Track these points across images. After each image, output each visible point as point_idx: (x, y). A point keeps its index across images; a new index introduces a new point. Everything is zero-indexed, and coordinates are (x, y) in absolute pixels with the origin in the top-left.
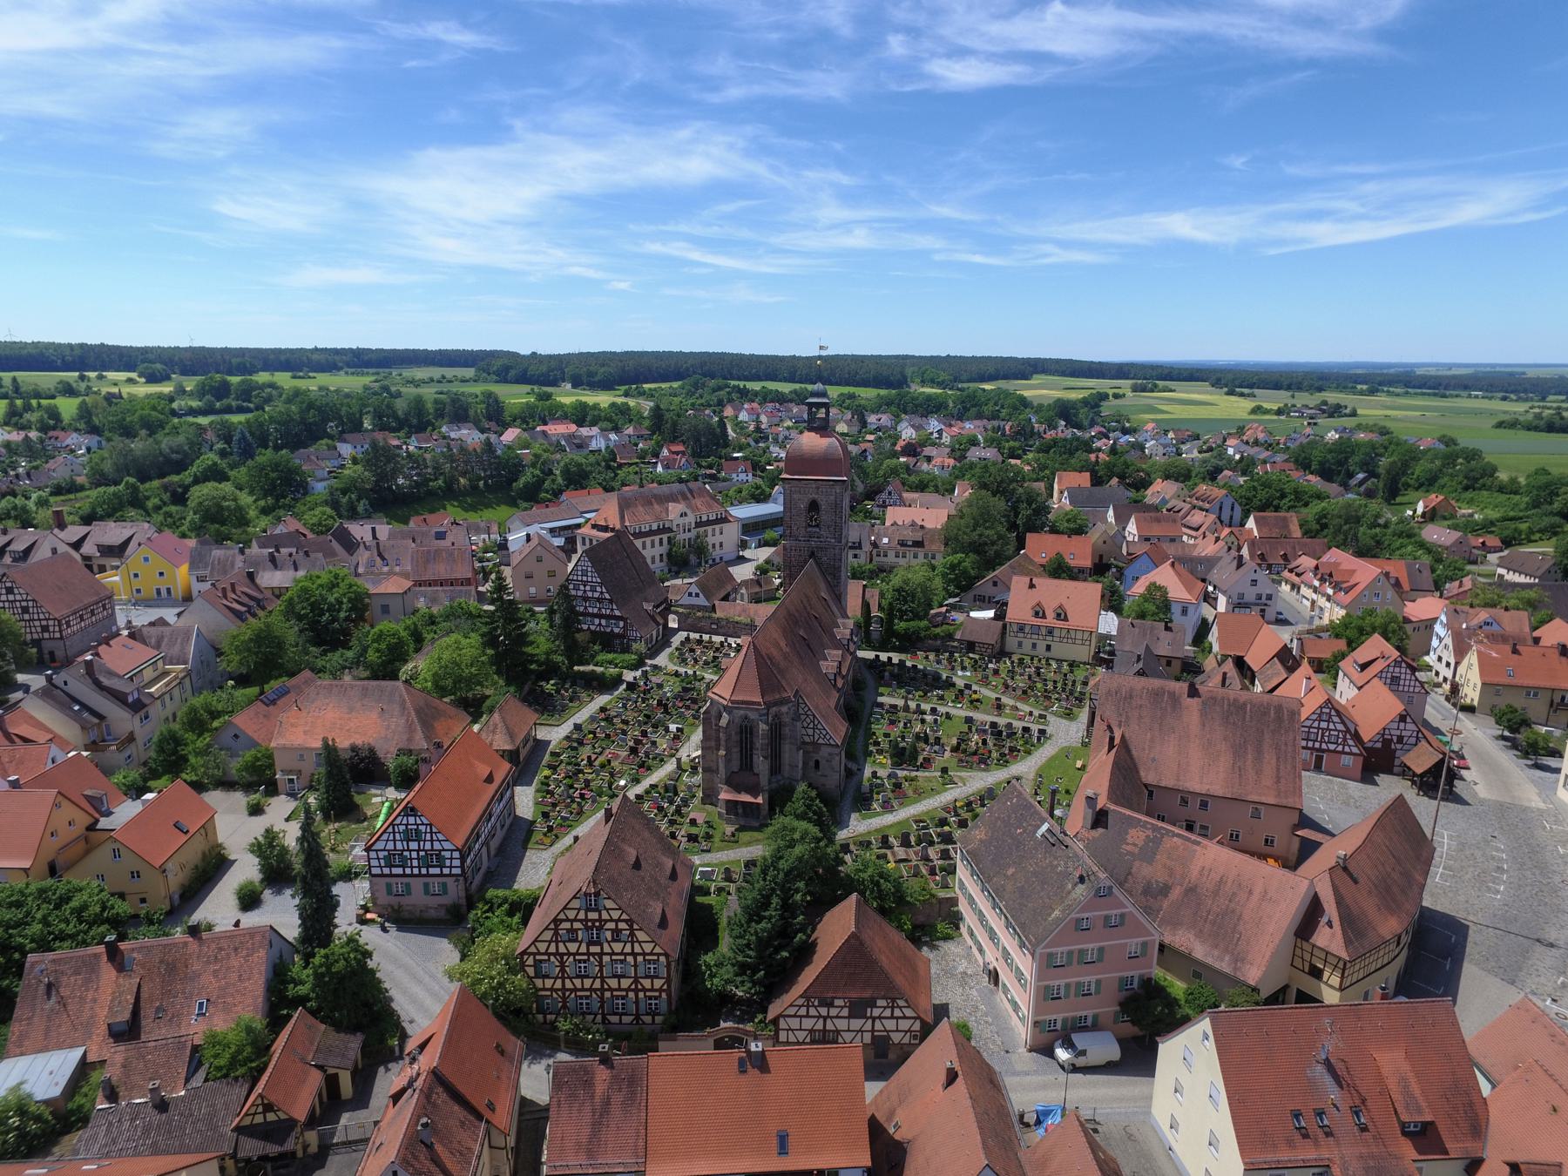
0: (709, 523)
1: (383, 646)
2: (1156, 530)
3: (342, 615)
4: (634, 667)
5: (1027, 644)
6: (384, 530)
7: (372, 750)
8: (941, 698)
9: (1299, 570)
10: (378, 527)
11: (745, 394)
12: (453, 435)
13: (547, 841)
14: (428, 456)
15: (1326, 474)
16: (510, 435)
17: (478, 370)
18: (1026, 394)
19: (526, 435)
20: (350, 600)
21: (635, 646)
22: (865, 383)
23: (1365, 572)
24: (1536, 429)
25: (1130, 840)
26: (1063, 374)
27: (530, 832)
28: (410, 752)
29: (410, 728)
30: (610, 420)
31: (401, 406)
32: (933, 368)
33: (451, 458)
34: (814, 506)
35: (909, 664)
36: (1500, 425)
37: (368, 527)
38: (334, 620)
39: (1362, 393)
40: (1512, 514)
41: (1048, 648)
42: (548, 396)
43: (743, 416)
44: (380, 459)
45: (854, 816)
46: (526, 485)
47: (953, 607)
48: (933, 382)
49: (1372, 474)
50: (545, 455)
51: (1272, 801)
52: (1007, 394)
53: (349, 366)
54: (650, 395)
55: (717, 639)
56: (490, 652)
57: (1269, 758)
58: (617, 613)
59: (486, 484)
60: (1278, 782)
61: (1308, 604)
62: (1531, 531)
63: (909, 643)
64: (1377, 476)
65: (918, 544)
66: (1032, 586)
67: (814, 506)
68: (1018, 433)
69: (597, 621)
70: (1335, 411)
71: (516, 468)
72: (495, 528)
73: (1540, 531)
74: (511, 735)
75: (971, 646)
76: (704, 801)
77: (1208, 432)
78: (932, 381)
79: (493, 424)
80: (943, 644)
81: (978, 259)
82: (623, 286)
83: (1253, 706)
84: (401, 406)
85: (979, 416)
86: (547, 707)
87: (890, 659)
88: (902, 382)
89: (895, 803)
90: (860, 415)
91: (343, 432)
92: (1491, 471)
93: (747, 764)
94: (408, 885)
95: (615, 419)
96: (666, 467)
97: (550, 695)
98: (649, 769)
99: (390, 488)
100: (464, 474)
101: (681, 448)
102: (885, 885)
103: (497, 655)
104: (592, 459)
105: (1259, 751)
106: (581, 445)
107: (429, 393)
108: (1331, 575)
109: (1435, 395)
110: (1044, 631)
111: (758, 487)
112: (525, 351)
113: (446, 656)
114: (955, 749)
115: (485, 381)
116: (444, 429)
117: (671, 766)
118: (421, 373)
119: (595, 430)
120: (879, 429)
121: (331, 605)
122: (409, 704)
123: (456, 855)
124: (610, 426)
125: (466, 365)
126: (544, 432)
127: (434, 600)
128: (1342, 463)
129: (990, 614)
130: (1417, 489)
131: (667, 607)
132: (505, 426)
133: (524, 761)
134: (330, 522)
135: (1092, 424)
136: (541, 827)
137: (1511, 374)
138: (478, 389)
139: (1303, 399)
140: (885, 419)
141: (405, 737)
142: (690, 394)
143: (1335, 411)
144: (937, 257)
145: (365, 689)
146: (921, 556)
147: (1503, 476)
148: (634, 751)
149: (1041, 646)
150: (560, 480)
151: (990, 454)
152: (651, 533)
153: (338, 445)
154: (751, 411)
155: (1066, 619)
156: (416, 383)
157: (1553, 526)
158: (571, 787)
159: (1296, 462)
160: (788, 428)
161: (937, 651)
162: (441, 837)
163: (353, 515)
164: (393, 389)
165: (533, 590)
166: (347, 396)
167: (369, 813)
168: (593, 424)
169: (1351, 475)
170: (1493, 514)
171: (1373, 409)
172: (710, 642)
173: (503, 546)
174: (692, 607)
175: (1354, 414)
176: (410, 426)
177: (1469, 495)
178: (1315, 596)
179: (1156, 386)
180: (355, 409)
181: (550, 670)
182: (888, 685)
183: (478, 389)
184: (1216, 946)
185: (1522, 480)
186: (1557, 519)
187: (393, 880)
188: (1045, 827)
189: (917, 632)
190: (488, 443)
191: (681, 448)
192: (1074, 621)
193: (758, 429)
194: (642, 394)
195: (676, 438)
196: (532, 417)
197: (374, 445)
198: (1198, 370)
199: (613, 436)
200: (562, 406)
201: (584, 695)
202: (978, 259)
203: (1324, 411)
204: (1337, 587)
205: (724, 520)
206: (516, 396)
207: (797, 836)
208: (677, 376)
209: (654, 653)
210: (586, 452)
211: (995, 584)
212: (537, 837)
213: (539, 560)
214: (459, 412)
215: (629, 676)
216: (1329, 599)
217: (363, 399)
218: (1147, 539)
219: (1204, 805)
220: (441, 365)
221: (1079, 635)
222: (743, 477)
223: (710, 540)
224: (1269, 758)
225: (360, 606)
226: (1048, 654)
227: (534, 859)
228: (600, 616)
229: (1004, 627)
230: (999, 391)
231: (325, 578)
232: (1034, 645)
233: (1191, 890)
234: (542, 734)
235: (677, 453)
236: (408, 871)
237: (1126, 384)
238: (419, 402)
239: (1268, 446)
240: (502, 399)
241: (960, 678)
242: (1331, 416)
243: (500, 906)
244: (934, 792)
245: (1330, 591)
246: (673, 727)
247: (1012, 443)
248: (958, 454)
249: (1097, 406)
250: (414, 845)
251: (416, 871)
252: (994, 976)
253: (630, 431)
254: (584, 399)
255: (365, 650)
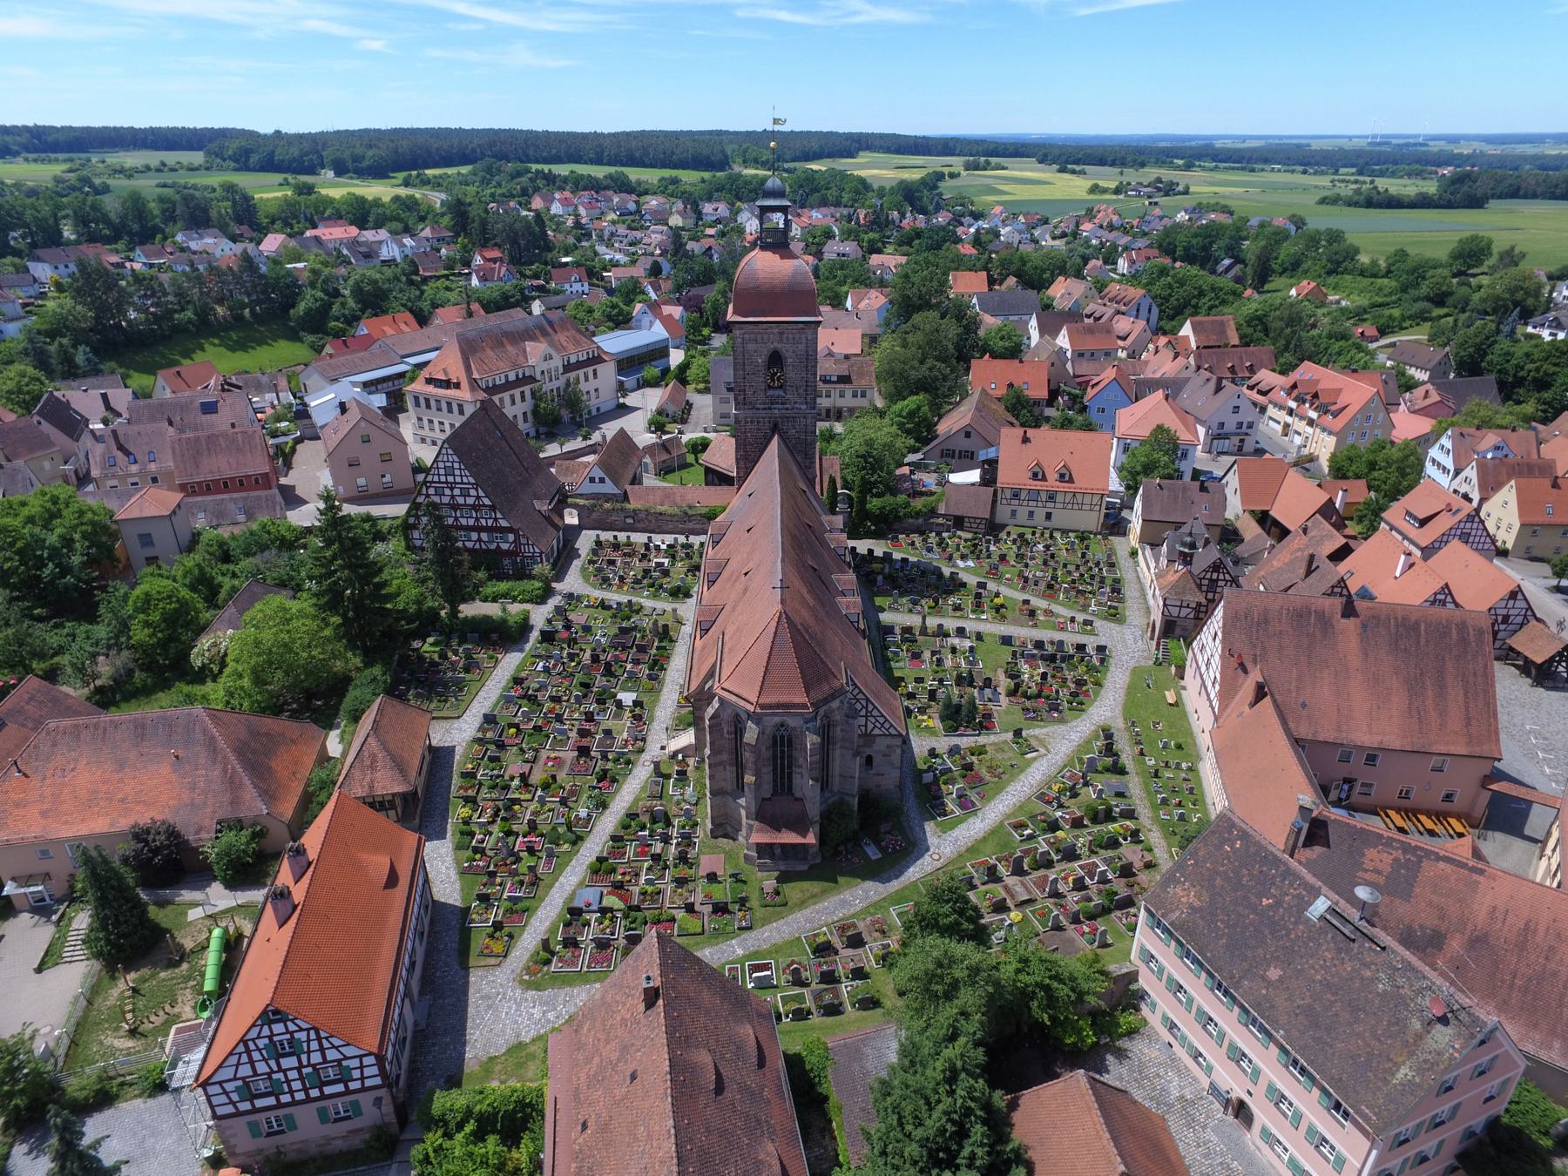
0: (580, 365)
1: (155, 617)
2: (1090, 344)
3: (76, 560)
4: (541, 600)
5: (1022, 514)
6: (121, 398)
7: (173, 834)
8: (957, 608)
9: (1263, 386)
10: (110, 392)
11: (550, 179)
12: (194, 245)
13: (498, 947)
14: (165, 278)
15: (1189, 258)
16: (272, 243)
17: (208, 153)
18: (862, 173)
19: (293, 243)
20: (85, 536)
21: (537, 569)
22: (682, 165)
23: (1356, 392)
24: (1356, 204)
25: (1368, 865)
26: (888, 151)
27: (465, 934)
28: (239, 825)
29: (233, 785)
30: (397, 218)
31: (112, 205)
32: (752, 144)
33: (199, 280)
34: (775, 359)
35: (879, 553)
36: (1323, 201)
37: (96, 394)
38: (65, 570)
39: (1178, 168)
40: (1380, 300)
41: (1049, 516)
42: (309, 190)
43: (556, 209)
44: (92, 284)
45: (929, 827)
46: (308, 312)
47: (916, 466)
48: (757, 163)
49: (1238, 260)
50: (327, 271)
51: (1462, 750)
52: (843, 175)
53: (28, 151)
54: (436, 184)
55: (639, 538)
56: (336, 620)
57: (1455, 694)
58: (504, 523)
59: (253, 312)
60: (1468, 724)
61: (1279, 428)
62: (1404, 318)
63: (886, 525)
64: (1243, 262)
65: (845, 379)
66: (1026, 440)
67: (775, 359)
68: (873, 222)
69: (474, 536)
70: (1169, 189)
71: (289, 290)
72: (283, 383)
73: (1410, 317)
74: (400, 767)
75: (959, 522)
76: (715, 835)
77: (1057, 215)
78: (756, 161)
79: (245, 228)
80: (924, 523)
81: (784, 16)
82: (377, 45)
83: (1428, 625)
84: (112, 205)
85: (824, 203)
86: (428, 684)
87: (871, 551)
88: (723, 164)
89: (972, 796)
90: (693, 204)
91: (34, 245)
92: (1352, 253)
93: (782, 783)
94: (289, 1118)
95: (404, 217)
96: (483, 279)
97: (433, 664)
98: (614, 780)
99: (118, 326)
100: (220, 301)
101: (496, 254)
102: (1063, 991)
103: (347, 621)
104: (388, 272)
105: (1441, 687)
106: (369, 254)
107: (147, 186)
108: (1315, 396)
109: (1243, 169)
110: (1044, 496)
111: (614, 306)
112: (265, 128)
113: (267, 636)
114: (1012, 693)
115: (221, 169)
116: (179, 238)
117: (641, 774)
118: (132, 159)
119: (383, 234)
120: (718, 221)
121: (53, 549)
122: (222, 744)
123: (370, 1060)
124: (400, 226)
125: (190, 146)
126: (317, 238)
127: (219, 517)
128: (1206, 248)
129: (974, 476)
130: (1281, 274)
131: (562, 499)
132: (261, 231)
133: (420, 809)
134: (36, 387)
135: (938, 209)
136: (482, 922)
137: (1298, 146)
138: (215, 179)
139: (1132, 176)
140: (723, 209)
141: (227, 798)
142: (485, 182)
143: (1169, 189)
144: (740, 14)
145: (140, 729)
146: (849, 394)
147: (1364, 259)
148: (584, 751)
149: (1040, 515)
150: (351, 303)
151: (849, 248)
152: (508, 386)
153: (31, 265)
154: (565, 202)
155: (1071, 481)
156: (129, 173)
157: (1423, 311)
158: (509, 833)
159: (1160, 247)
160: (613, 222)
161: (921, 532)
162: (336, 1042)
163: (71, 372)
164: (97, 181)
165: (361, 481)
166: (32, 193)
167: (188, 944)
168: (378, 225)
169: (1217, 261)
170: (1363, 301)
171: (1204, 185)
172: (629, 544)
173: (302, 414)
174: (596, 496)
175: (1186, 192)
176: (130, 234)
177: (1332, 280)
178: (1289, 419)
179: (988, 163)
180: (46, 210)
181: (427, 622)
182: (885, 593)
183: (215, 179)
184: (1535, 1026)
185: (1382, 263)
186: (1426, 305)
187: (263, 1116)
188: (1320, 906)
189: (894, 511)
190: (247, 259)
191: (496, 254)
192: (1081, 483)
193: (578, 225)
194: (426, 182)
195: (487, 241)
196: (295, 217)
197: (82, 266)
198: (1024, 145)
199: (408, 241)
200: (331, 201)
201: (482, 656)
202: (784, 16)
203: (1159, 189)
204: (1323, 410)
205: (596, 359)
206: (269, 191)
207: (959, 973)
208: (464, 159)
209: (560, 571)
210: (377, 262)
211: (968, 435)
212: (479, 941)
213: (366, 440)
214: (199, 219)
215: (540, 616)
216: (1311, 423)
217: (61, 189)
218: (1081, 355)
219: (1371, 759)
220: (157, 148)
221: (1087, 499)
222: (577, 287)
223: (583, 386)
224: (1455, 694)
225: (106, 551)
226: (1048, 524)
227: (486, 990)
228: (479, 529)
229: (995, 492)
230: (833, 173)
231: (35, 506)
232: (1031, 514)
233: (1478, 941)
234: (440, 735)
235: (494, 260)
236: (285, 1098)
237: (957, 163)
238: (136, 204)
239: (1125, 230)
240: (250, 192)
241: (967, 570)
242: (1167, 194)
243: (460, 1127)
244: (1016, 769)
245: (1313, 415)
246: (627, 698)
247: (871, 235)
248: (813, 249)
249: (935, 187)
250: (287, 1062)
251: (300, 1096)
252: (1241, 1111)
253: (427, 232)
254: (353, 190)
255: (124, 627)
